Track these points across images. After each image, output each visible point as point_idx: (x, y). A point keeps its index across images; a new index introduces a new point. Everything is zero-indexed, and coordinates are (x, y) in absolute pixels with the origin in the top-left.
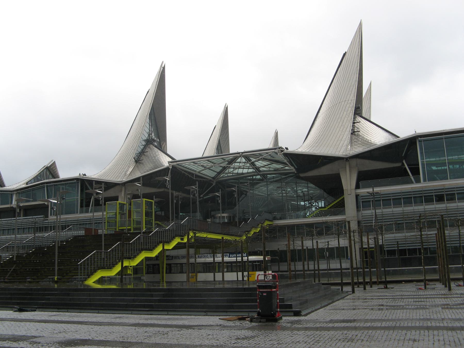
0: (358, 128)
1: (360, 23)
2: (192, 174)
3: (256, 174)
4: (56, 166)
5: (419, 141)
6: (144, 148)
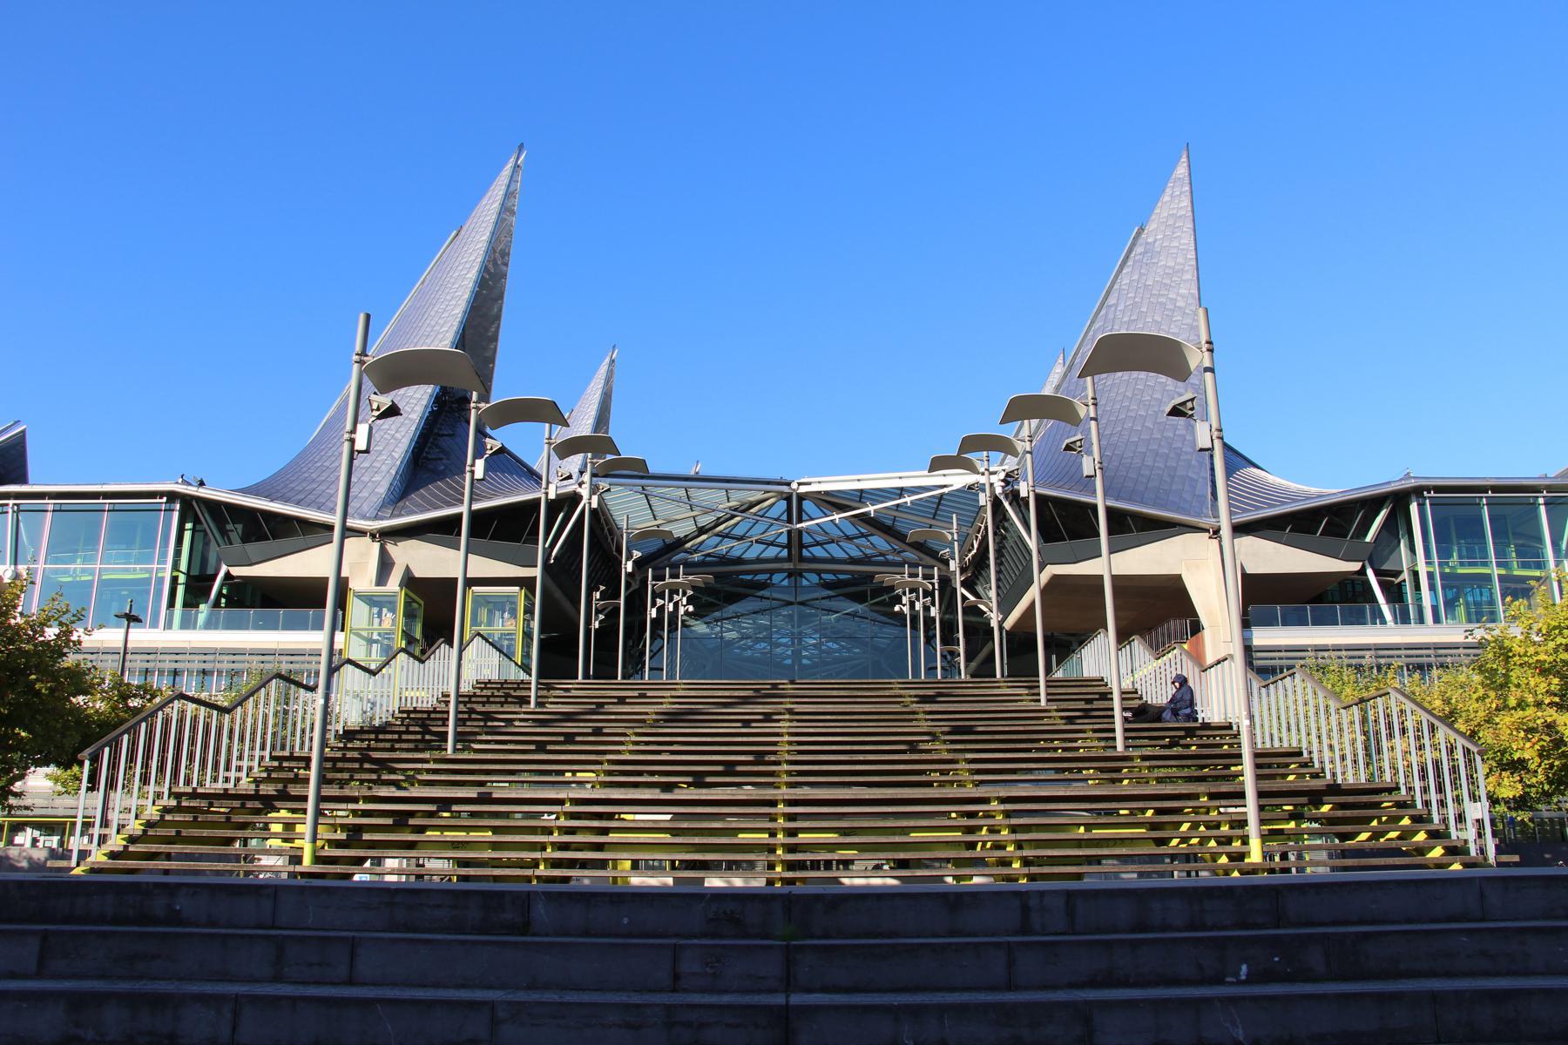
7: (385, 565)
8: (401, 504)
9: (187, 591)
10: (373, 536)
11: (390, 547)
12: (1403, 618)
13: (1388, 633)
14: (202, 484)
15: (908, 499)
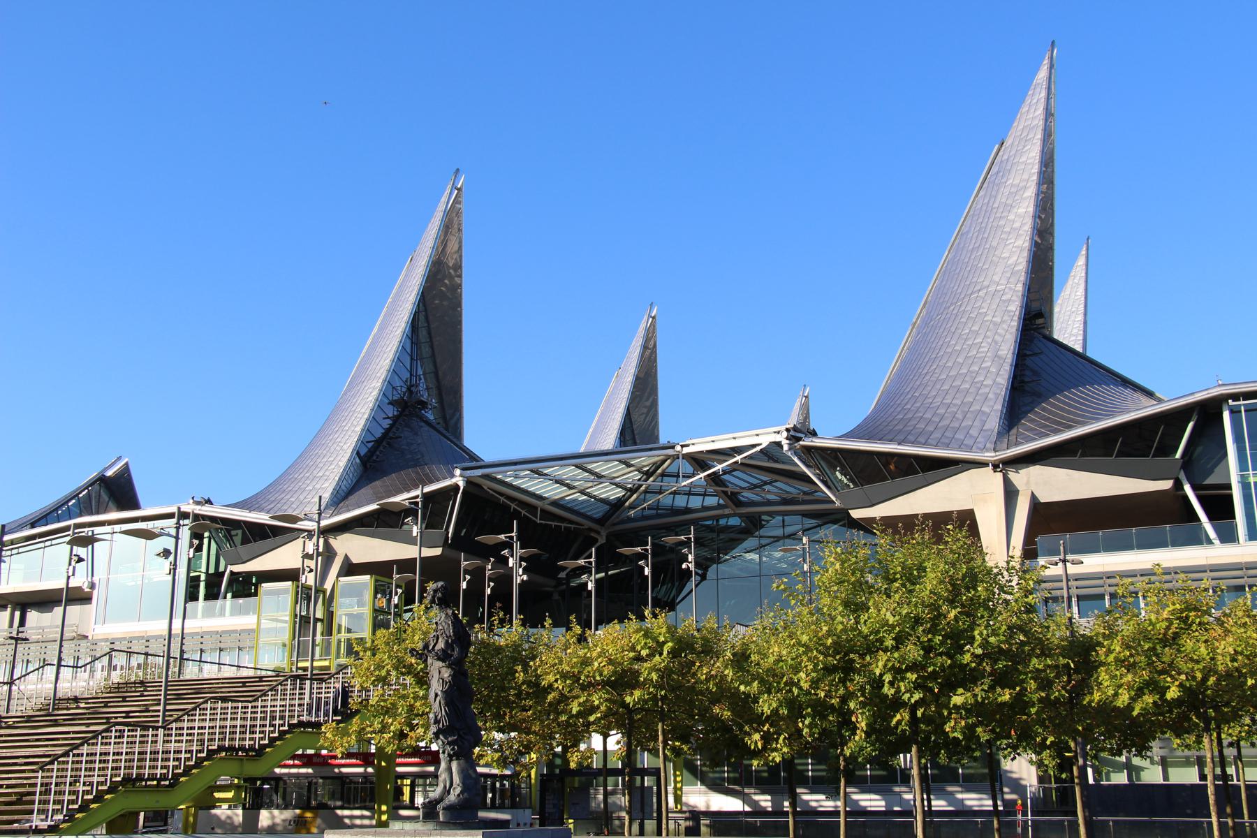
0: (1035, 373)
1: (1126, 382)
2: (532, 508)
3: (727, 511)
4: (130, 475)
5: (1232, 412)
6: (392, 426)
7: (1011, 494)
8: (1014, 431)
9: (207, 587)
10: (995, 467)
11: (1012, 476)
12: (1228, 536)
13: (1215, 553)
14: (209, 502)
15: (738, 458)
